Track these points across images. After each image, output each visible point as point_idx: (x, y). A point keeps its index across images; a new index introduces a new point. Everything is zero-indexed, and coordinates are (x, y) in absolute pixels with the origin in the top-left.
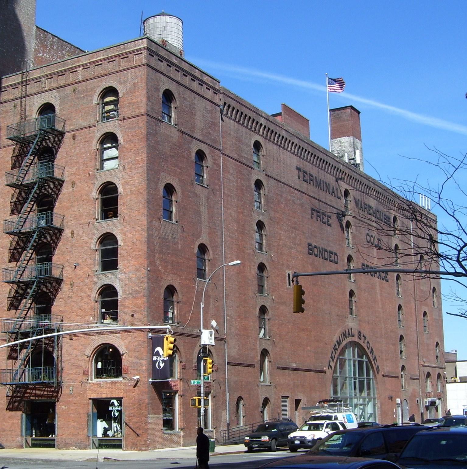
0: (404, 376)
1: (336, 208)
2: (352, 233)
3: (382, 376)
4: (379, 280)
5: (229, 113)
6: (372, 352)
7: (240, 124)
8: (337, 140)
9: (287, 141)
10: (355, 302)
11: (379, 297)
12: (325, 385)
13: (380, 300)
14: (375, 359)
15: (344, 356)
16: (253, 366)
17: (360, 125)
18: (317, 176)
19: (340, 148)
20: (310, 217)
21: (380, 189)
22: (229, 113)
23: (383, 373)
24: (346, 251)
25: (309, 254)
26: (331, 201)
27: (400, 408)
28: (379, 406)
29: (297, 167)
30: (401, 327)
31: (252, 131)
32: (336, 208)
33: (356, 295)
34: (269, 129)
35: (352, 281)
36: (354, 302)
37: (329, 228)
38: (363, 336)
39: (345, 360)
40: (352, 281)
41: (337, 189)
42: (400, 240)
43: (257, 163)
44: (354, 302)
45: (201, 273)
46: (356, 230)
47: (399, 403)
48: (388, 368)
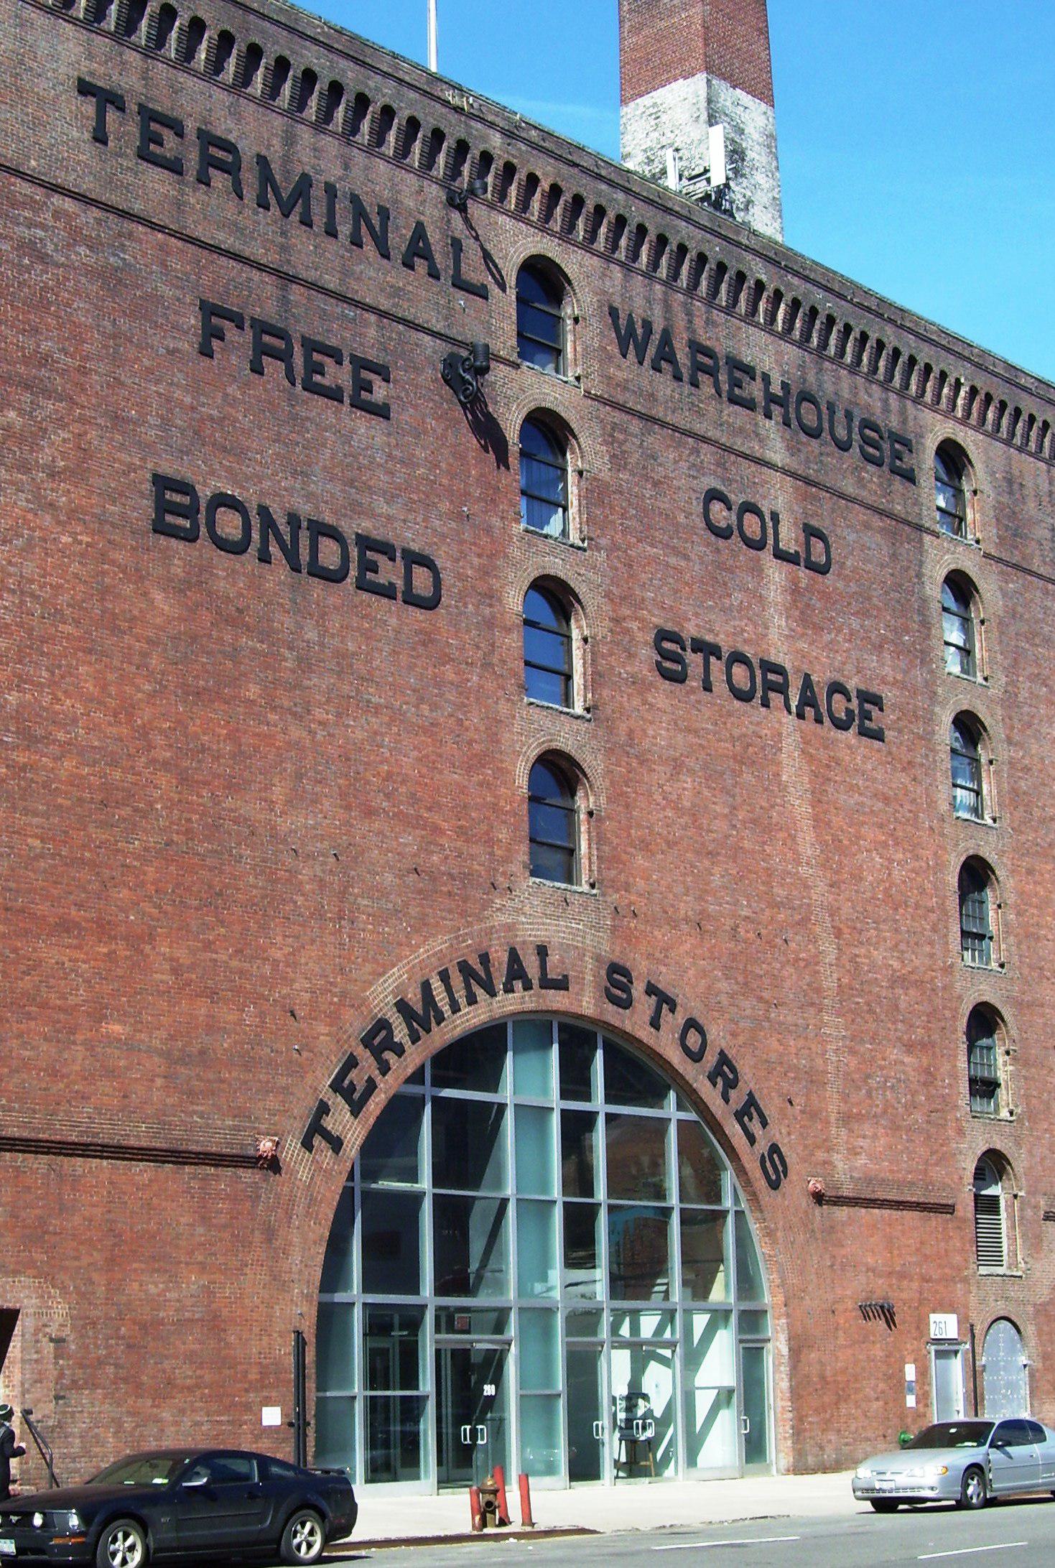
0: (1010, 1207)
1: (435, 334)
2: (580, 473)
3: (805, 1202)
4: (809, 725)
5: (704, 283)
6: (725, 1073)
7: (842, 365)
8: (646, 101)
9: (818, 325)
10: (590, 814)
11: (801, 807)
12: (270, 1234)
13: (806, 824)
14: (750, 1109)
15: (496, 1091)
16: (948, 1209)
17: (764, 32)
18: (275, 153)
19: (656, 135)
20: (188, 345)
21: (820, 294)
22: (815, 336)
23: (815, 1184)
24: (515, 552)
25: (160, 528)
26: (397, 292)
27: (956, 1366)
28: (785, 1350)
29: (80, 80)
30: (994, 965)
31: (1030, 454)
32: (435, 334)
33: (597, 783)
34: (880, 345)
35: (578, 709)
36: (583, 816)
37: (364, 427)
38: (651, 990)
39: (502, 1107)
40: (578, 709)
41: (457, 245)
42: (987, 556)
43: (955, 516)
44: (583, 816)
45: (974, 937)
46: (618, 461)
47: (952, 1333)
48: (862, 1161)
